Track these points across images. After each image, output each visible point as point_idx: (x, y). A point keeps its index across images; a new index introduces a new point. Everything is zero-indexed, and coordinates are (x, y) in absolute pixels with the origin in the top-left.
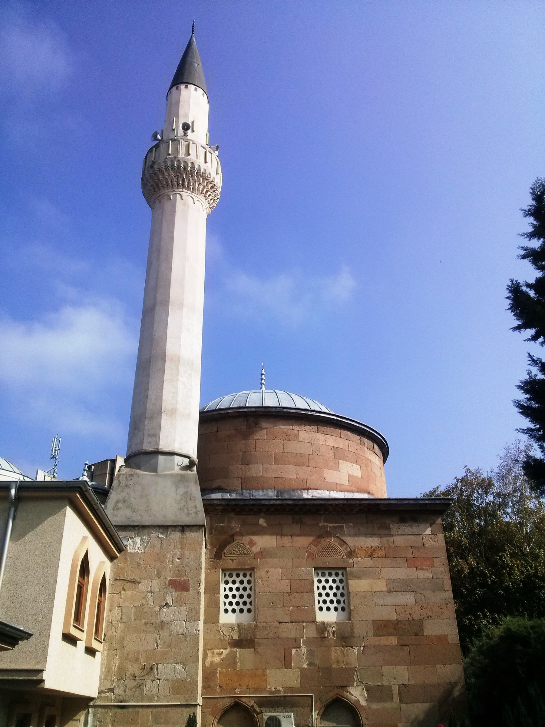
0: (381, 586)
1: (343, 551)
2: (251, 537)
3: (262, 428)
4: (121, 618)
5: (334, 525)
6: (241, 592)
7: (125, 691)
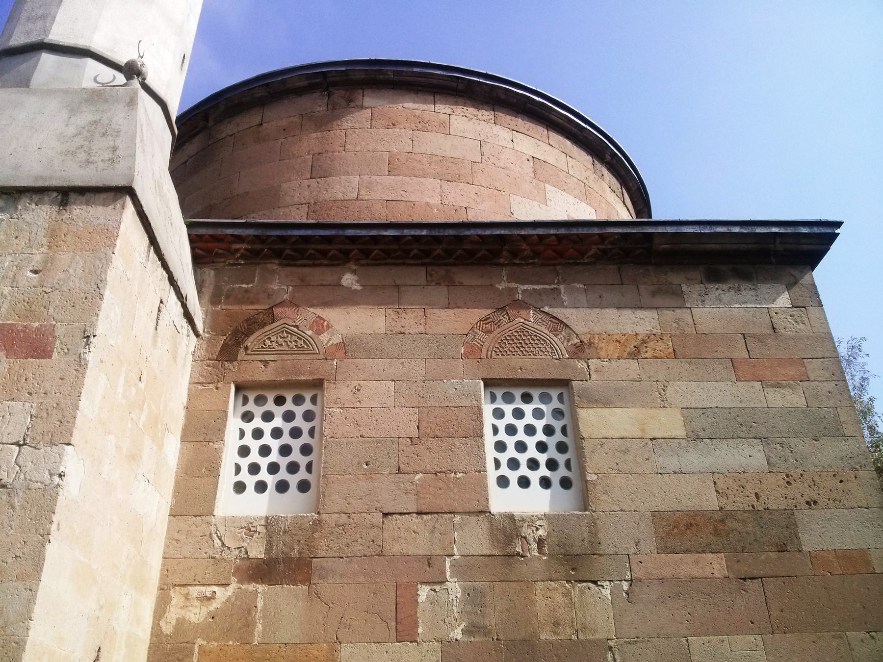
0: (669, 423)
1: (559, 342)
2: (319, 311)
3: (362, 107)
5: (536, 287)
6: (286, 439)
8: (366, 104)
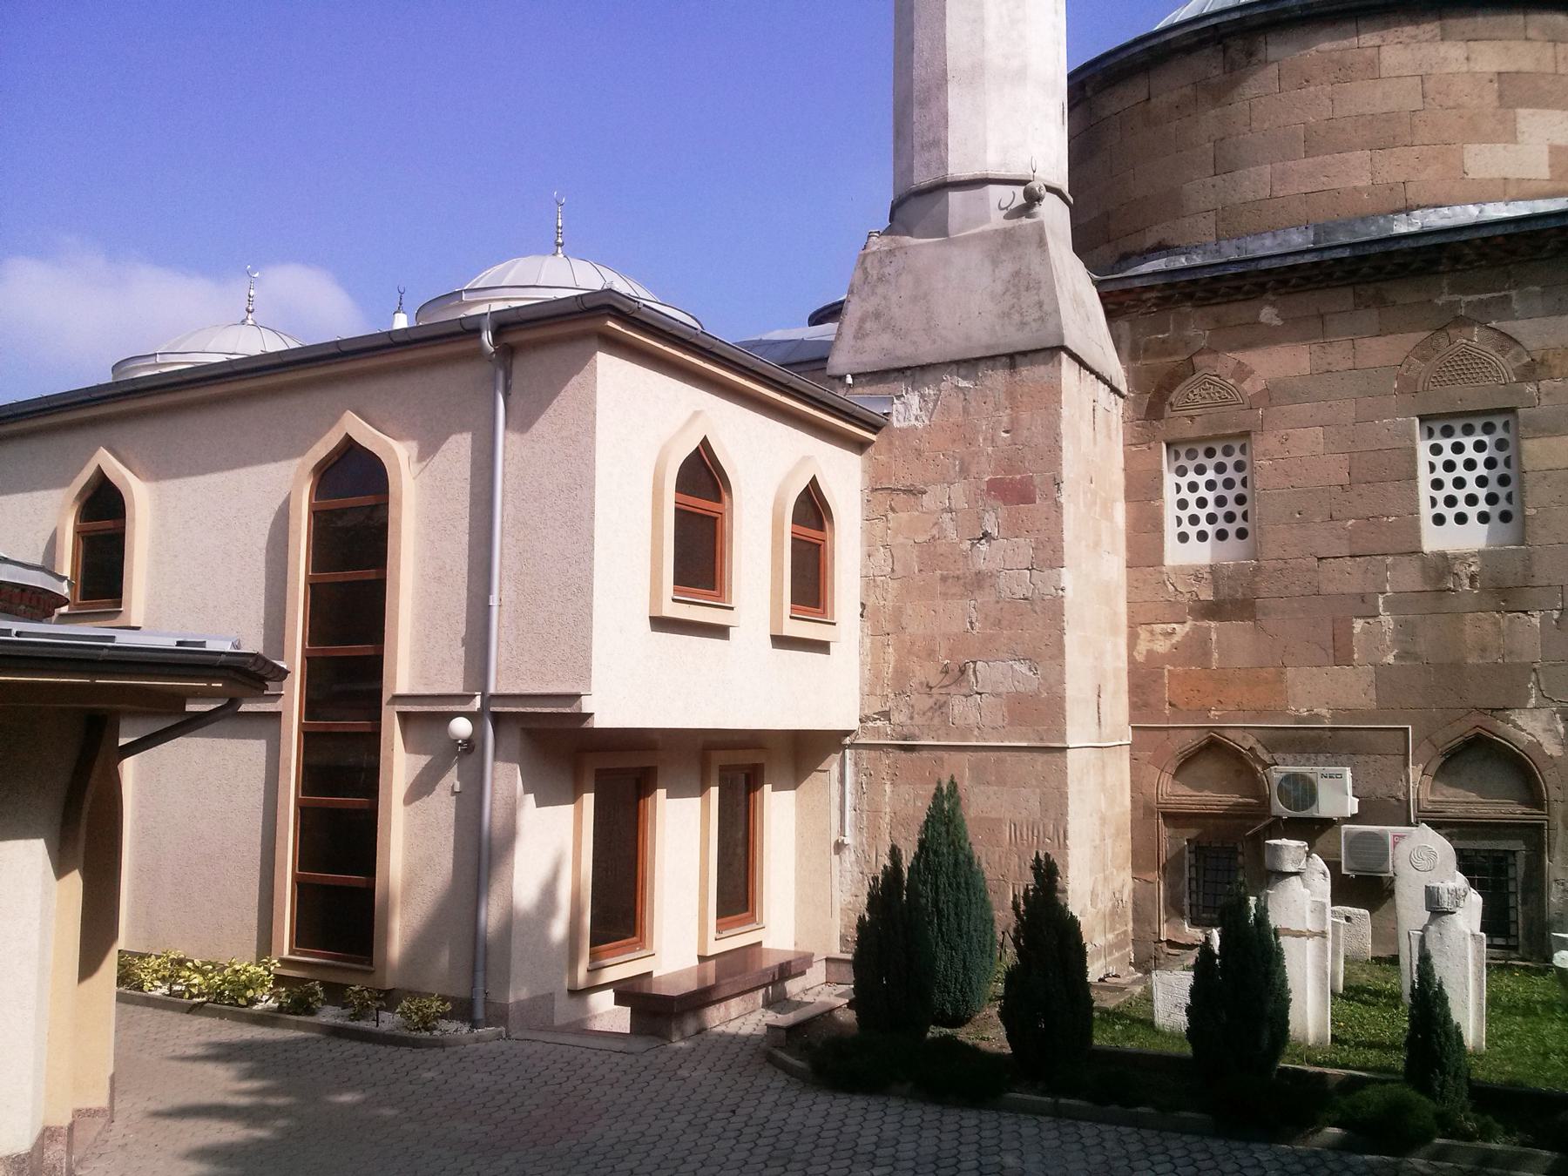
1: (1507, 364)
2: (1239, 356)
3: (1266, 63)
6: (1220, 490)
8: (1271, 58)
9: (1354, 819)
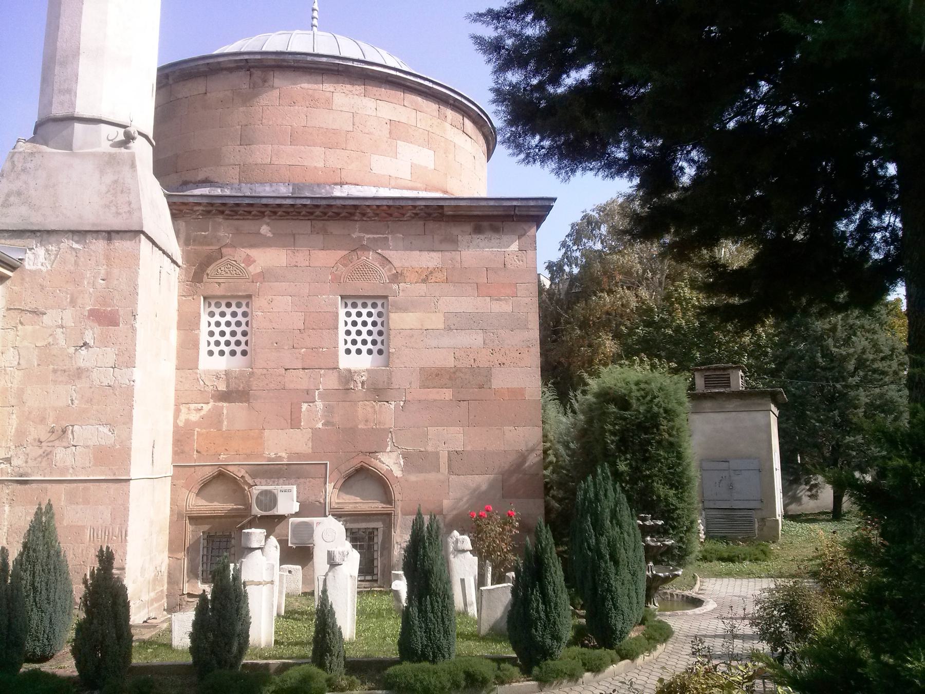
0: (436, 321)
1: (385, 273)
3: (273, 87)
4: (19, 364)
5: (375, 236)
6: (233, 327)
7: (26, 462)
9: (297, 515)
